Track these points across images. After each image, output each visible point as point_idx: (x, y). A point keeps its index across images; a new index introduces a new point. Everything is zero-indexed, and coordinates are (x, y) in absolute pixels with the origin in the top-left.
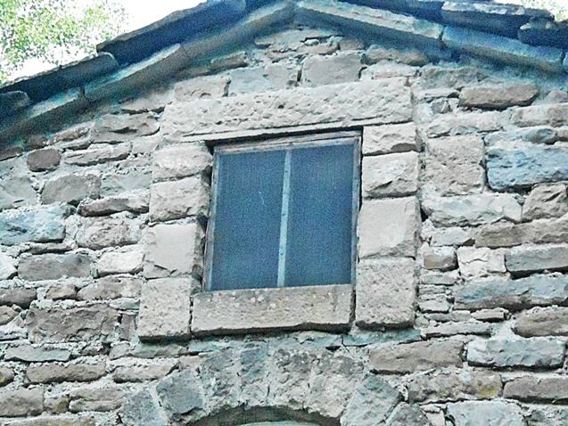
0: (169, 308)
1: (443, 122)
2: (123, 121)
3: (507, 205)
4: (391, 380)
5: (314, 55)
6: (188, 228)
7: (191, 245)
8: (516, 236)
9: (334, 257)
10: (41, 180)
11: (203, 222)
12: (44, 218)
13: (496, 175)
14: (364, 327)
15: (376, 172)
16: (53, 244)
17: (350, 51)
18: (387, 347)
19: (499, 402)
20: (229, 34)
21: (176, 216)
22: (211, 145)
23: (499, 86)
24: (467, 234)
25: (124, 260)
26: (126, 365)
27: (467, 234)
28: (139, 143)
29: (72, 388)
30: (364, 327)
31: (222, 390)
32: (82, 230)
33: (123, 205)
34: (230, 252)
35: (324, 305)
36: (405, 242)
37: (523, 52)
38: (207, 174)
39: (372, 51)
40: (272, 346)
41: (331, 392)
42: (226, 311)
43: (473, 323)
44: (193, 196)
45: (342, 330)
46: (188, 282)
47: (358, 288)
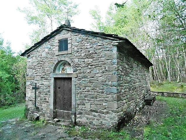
0: (57, 53)
1: (73, 37)
2: (54, 38)
3: (77, 44)
4: (70, 58)
5: (65, 32)
6: (58, 47)
7: (58, 48)
8: (78, 46)
9: (66, 49)
10: (49, 43)
11: (59, 46)
12: (49, 46)
13: (77, 41)
14: (69, 54)
15: (69, 42)
16: (50, 48)
17: (67, 32)
18: (70, 55)
19: (77, 59)
20: (59, 31)
21: (57, 46)
22: (59, 40)
23: (76, 34)
24: (75, 46)
25: (54, 49)
26: (55, 57)
27: (75, 46)
28: (54, 40)
29: (52, 59)
30: (69, 54)
31: (60, 59)
32: (52, 47)
33: (54, 45)
34: (60, 49)
35: (65, 52)
36: (64, 25)
37: (77, 31)
38: (59, 42)
39: (69, 32)
40: (63, 55)
41: (67, 59)
42: (61, 53)
43: (75, 53)
44: (58, 44)
45: (67, 54)
46: (58, 51)
47: (164, 92)
